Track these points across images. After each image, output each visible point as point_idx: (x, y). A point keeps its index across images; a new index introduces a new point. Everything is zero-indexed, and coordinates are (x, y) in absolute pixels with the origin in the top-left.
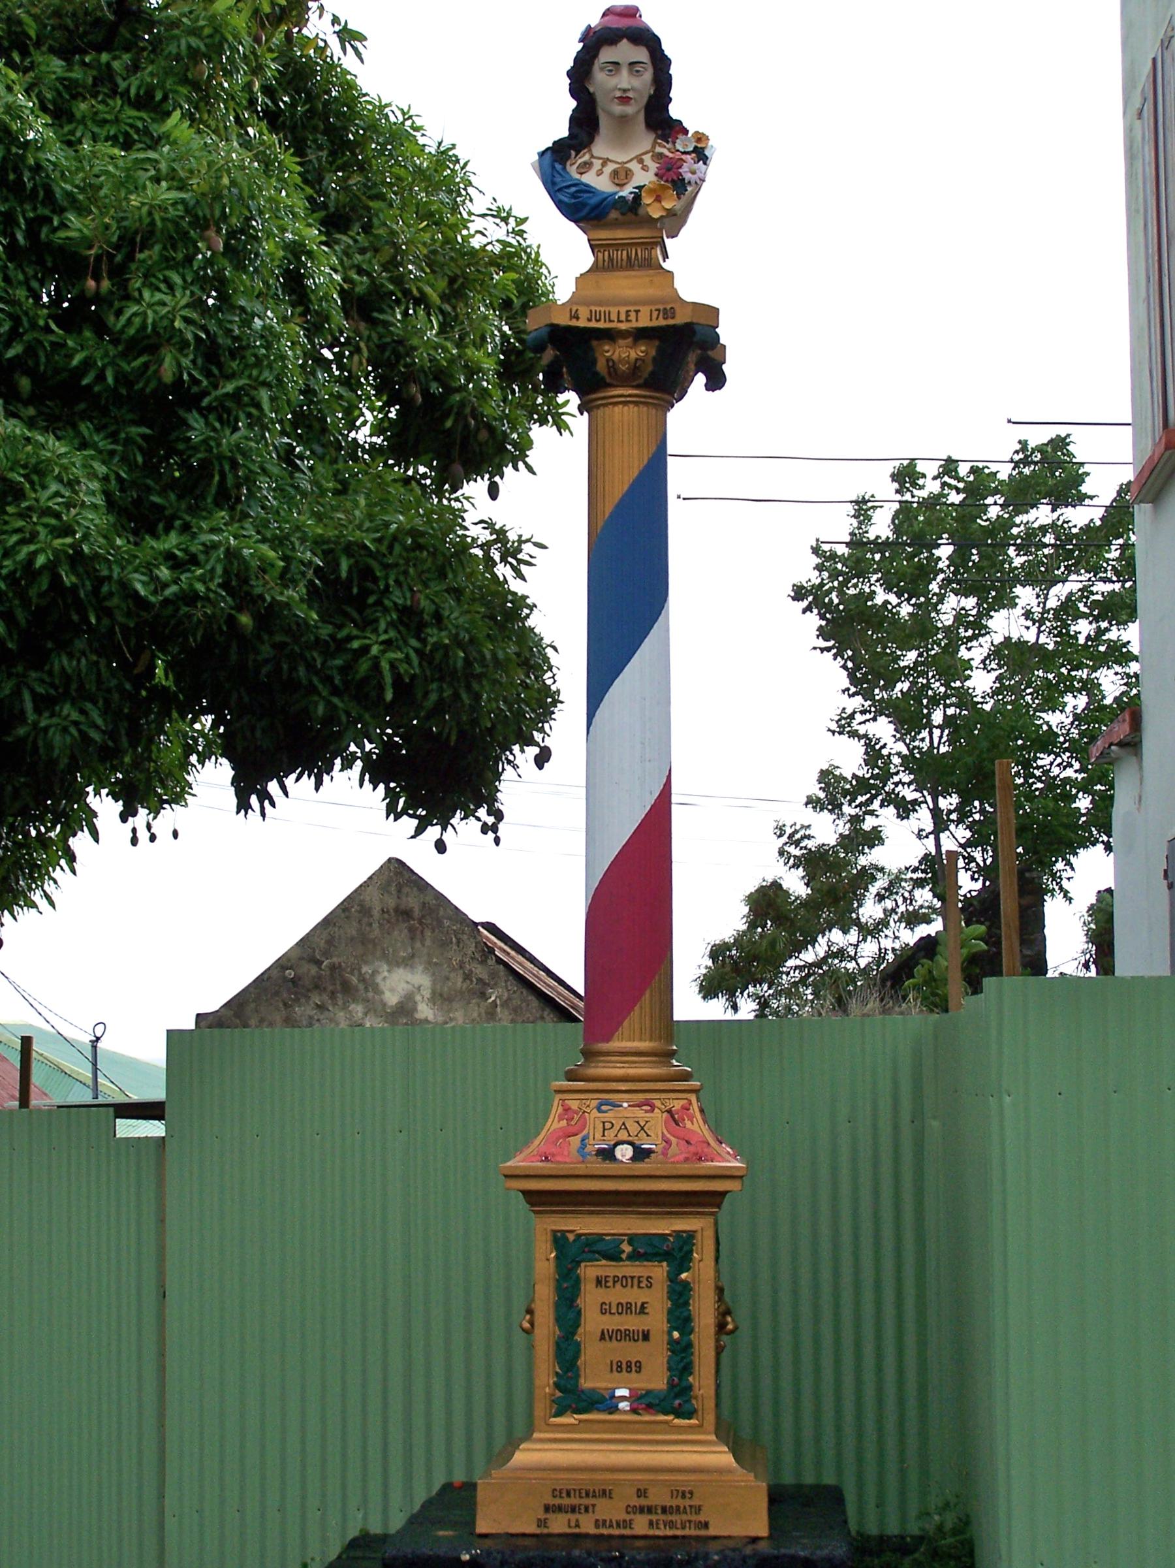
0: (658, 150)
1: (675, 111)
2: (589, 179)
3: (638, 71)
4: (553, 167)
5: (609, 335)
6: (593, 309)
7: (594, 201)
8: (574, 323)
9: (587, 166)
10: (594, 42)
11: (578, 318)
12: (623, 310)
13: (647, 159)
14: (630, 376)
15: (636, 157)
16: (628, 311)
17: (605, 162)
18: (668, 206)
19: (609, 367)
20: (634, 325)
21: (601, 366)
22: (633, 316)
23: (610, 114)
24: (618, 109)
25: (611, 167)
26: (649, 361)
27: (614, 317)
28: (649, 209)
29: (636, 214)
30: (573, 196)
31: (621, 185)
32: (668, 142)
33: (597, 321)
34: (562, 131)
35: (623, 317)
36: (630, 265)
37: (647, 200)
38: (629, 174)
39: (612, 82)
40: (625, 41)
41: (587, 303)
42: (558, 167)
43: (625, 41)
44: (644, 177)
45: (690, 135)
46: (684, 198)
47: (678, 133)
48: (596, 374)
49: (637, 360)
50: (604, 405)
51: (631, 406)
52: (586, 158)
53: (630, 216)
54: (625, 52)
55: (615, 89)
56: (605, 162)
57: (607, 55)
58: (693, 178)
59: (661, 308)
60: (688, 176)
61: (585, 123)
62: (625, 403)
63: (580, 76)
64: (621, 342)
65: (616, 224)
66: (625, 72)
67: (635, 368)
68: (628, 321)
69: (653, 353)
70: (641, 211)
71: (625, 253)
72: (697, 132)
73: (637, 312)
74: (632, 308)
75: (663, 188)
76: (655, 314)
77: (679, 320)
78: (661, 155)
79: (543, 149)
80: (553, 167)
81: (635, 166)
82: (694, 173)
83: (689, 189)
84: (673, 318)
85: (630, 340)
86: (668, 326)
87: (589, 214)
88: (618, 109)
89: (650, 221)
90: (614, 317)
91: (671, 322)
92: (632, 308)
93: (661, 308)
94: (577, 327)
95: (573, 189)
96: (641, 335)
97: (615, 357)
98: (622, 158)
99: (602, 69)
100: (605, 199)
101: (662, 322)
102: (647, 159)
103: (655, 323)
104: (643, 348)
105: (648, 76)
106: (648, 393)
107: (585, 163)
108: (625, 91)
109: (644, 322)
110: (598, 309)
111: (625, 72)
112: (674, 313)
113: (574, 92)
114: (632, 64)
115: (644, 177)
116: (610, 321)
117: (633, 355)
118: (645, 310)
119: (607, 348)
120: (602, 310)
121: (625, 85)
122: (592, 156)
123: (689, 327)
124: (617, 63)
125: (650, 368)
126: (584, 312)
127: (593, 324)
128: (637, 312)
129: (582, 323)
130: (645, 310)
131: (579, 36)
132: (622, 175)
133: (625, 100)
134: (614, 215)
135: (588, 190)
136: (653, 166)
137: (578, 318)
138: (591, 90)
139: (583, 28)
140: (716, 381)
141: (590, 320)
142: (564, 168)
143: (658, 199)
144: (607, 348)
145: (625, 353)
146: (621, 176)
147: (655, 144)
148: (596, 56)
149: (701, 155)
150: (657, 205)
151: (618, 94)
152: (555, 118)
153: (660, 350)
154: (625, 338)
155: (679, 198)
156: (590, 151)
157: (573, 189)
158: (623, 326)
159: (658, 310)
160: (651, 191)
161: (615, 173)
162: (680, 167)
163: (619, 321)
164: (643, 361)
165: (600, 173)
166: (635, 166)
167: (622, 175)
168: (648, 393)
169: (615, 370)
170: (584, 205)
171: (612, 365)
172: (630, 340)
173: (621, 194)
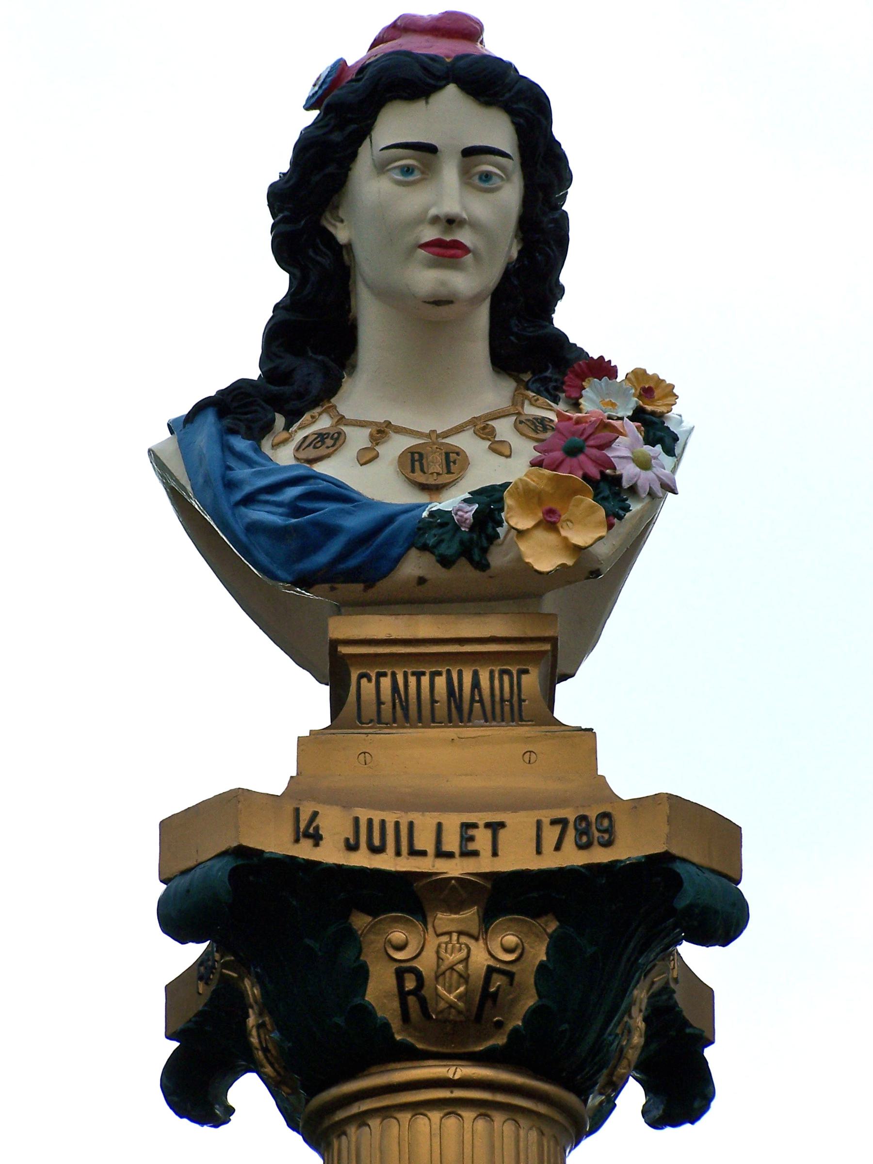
0: (531, 411)
1: (577, 318)
2: (336, 468)
3: (486, 177)
4: (227, 448)
5: (407, 897)
6: (364, 815)
7: (355, 522)
8: (305, 851)
9: (329, 442)
10: (348, 105)
11: (316, 838)
12: (452, 823)
13: (504, 428)
14: (463, 1025)
15: (473, 422)
16: (466, 826)
17: (382, 432)
18: (580, 538)
19: (403, 995)
20: (486, 864)
21: (380, 991)
22: (482, 840)
23: (393, 296)
24: (426, 279)
25: (396, 447)
26: (527, 975)
27: (425, 841)
28: (524, 547)
29: (483, 566)
30: (294, 509)
31: (434, 489)
32: (556, 400)
33: (376, 850)
34: (241, 359)
35: (451, 843)
36: (458, 711)
37: (517, 519)
38: (454, 462)
39: (413, 201)
40: (452, 90)
41: (344, 800)
42: (241, 444)
43: (452, 90)
44: (508, 464)
45: (621, 377)
46: (622, 528)
47: (582, 376)
48: (367, 1011)
49: (490, 970)
50: (385, 1112)
51: (468, 1115)
52: (324, 423)
53: (464, 571)
54: (451, 118)
55: (419, 220)
56: (382, 432)
57: (396, 125)
58: (645, 479)
59: (571, 815)
60: (628, 471)
61: (311, 340)
62: (450, 1106)
63: (306, 207)
64: (444, 919)
65: (418, 599)
66: (450, 172)
67: (487, 998)
68: (467, 854)
69: (539, 953)
70: (498, 558)
71: (441, 682)
72: (639, 375)
73: (495, 827)
74: (481, 818)
75: (569, 492)
76: (551, 835)
77: (627, 849)
78: (542, 424)
79: (184, 409)
80: (227, 448)
81: (467, 442)
82: (645, 464)
83: (636, 507)
84: (608, 844)
85: (470, 916)
86: (589, 867)
87: (342, 556)
88: (426, 279)
89: (525, 590)
90: (425, 841)
91: (600, 856)
92: (481, 818)
93: (571, 815)
94: (312, 865)
95: (292, 492)
96: (505, 896)
97: (426, 964)
98: (428, 422)
99: (382, 168)
100: (390, 519)
101: (572, 857)
102: (504, 428)
103: (551, 861)
104: (511, 939)
105: (510, 195)
106: (518, 1080)
107: (321, 437)
108: (451, 222)
109: (517, 856)
110: (377, 816)
111: (450, 172)
112: (610, 830)
113: (285, 249)
114: (469, 152)
115: (508, 464)
116: (414, 852)
117: (480, 959)
118: (519, 826)
119: (398, 935)
120: (390, 818)
121: (451, 205)
122: (341, 420)
123: (659, 869)
124: (431, 149)
125: (530, 1001)
126: (334, 824)
127: (362, 859)
128: (495, 827)
129: (330, 853)
130: (519, 826)
131: (306, 90)
132: (436, 464)
133: (447, 252)
134: (414, 566)
135: (339, 494)
136: (525, 450)
137: (316, 838)
138: (342, 235)
139: (321, 66)
140: (681, 1094)
141: (352, 847)
142: (258, 450)
143: (550, 522)
144: (398, 935)
145: (453, 952)
146: (431, 464)
147: (517, 401)
148: (364, 132)
149: (659, 433)
150: (542, 536)
151: (430, 234)
152: (228, 310)
153: (556, 945)
154: (455, 906)
155: (610, 526)
156: (332, 410)
157: (292, 492)
158: (454, 868)
159: (562, 822)
160: (529, 496)
161: (413, 460)
162: (608, 445)
163: (441, 854)
164: (510, 975)
165: (367, 457)
166: (467, 442)
167: (436, 464)
168: (518, 1080)
169: (423, 1003)
170: (330, 531)
171: (412, 987)
172: (470, 916)
173: (436, 506)
